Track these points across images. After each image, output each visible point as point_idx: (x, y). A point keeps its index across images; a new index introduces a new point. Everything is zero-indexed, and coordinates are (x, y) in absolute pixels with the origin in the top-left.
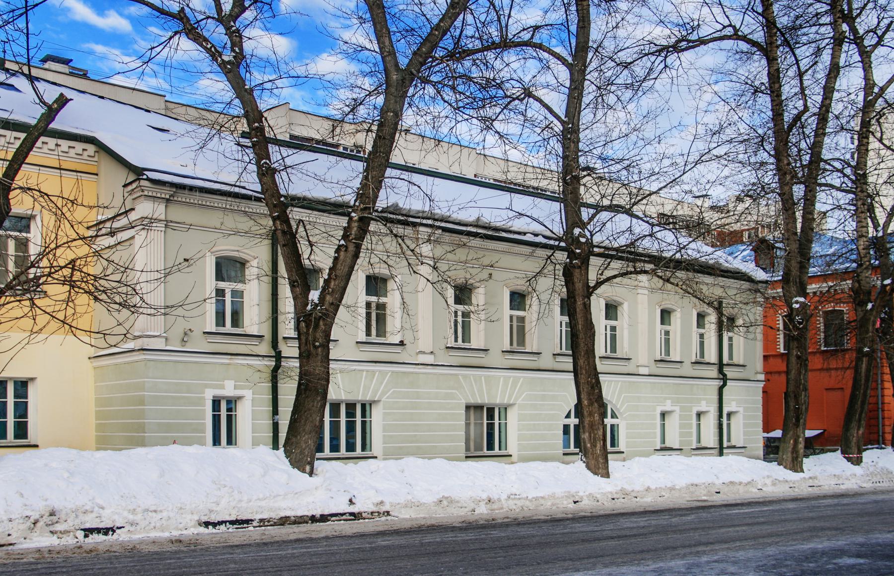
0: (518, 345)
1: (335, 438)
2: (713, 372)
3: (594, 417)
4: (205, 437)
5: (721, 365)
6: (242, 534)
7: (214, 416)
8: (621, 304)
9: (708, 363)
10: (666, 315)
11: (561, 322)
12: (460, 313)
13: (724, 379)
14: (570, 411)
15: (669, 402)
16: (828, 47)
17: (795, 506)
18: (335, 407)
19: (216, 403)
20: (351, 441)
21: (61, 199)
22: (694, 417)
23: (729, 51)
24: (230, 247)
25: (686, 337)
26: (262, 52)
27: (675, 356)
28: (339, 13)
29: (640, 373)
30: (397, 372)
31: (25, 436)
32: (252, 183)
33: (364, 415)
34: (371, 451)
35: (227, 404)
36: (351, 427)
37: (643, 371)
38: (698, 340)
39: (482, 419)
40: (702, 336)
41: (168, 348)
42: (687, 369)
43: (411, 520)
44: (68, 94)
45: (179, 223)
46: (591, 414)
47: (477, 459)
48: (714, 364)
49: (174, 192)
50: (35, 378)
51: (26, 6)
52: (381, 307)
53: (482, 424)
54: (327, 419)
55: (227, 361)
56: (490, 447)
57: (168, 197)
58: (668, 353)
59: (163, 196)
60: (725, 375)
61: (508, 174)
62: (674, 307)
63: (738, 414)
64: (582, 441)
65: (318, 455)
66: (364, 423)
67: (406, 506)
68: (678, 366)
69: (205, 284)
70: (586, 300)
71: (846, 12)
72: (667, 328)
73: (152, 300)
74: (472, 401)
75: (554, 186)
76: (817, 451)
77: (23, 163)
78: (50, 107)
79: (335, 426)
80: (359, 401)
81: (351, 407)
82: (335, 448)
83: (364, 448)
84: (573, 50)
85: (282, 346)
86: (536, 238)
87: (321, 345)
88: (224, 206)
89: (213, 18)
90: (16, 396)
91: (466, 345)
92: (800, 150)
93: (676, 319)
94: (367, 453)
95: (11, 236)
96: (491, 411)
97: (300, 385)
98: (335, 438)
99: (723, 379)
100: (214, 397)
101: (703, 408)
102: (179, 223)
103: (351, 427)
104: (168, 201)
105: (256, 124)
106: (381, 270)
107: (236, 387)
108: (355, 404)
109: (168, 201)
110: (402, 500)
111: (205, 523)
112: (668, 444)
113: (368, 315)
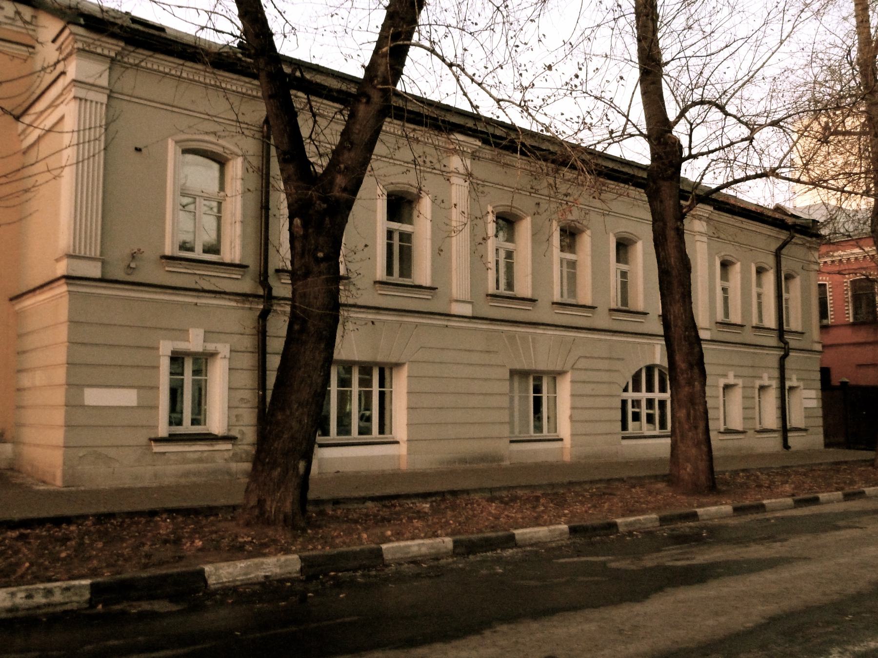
0: (402, 275)
1: (366, 419)
2: (773, 341)
3: (694, 386)
4: (371, 391)
5: (781, 332)
6: (196, 456)
7: (622, 282)
8: (418, 197)
9: (420, 287)
10: (725, 265)
11: (167, 271)
12: (396, 237)
13: (786, 351)
14: (628, 383)
15: (731, 374)
16: (804, 16)
17: (555, 293)
18: (347, 366)
19: (177, 359)
20: (537, 423)
21: (706, 87)
22: (165, 364)
23: (555, 177)
24: (626, 227)
25: (599, 273)
26: (170, 249)
27: (585, 296)
28: (19, 175)
29: (452, 313)
30: (548, 429)
31: (409, 276)
32: (795, 140)
33: (382, 384)
34: (391, 433)
35: (193, 363)
36: (366, 399)
37: (457, 309)
38: (619, 280)
39: (527, 391)
40: (624, 274)
41: (722, 417)
42: (602, 320)
43: (696, 263)
44: (540, 201)
45: (75, 234)
46: (690, 383)
47: (762, 410)
48: (773, 330)
49: (123, 49)
50: (537, 300)
51: (331, 121)
52: (406, 237)
53: (527, 397)
54: (334, 388)
55: (446, 323)
56: (538, 428)
57: (113, 54)
58: (573, 291)
59: (106, 52)
60: (786, 343)
61: (586, 131)
62: (734, 260)
63: (771, 388)
64: (183, 481)
65: (320, 439)
66: (382, 395)
67: (225, 137)
68: (426, 295)
69: (622, 298)
70: (679, 223)
71: (86, 537)
72: (726, 284)
73: (604, 389)
74: (518, 366)
75: (783, 235)
76: (408, 535)
77: (293, 299)
78: (509, 423)
79: (344, 399)
80: (376, 364)
81: (366, 369)
82: (344, 427)
83: (382, 431)
84: (269, 394)
85: (272, 281)
86: (128, 276)
87: (326, 259)
88: (179, 74)
89: (785, 244)
90: (360, 385)
91: (406, 281)
92: (829, 95)
93: (736, 271)
94: (387, 437)
95: (39, 589)
96: (538, 377)
97: (130, 489)
98: (366, 419)
99: (784, 348)
100: (173, 352)
101: (195, 342)
102: (141, 99)
103: (366, 399)
104: (113, 60)
105: (332, 573)
106: (405, 180)
107: (735, 376)
108: (369, 375)
109: (113, 60)
110: (40, 149)
111: (514, 150)
112: (110, 276)
113: (390, 247)
